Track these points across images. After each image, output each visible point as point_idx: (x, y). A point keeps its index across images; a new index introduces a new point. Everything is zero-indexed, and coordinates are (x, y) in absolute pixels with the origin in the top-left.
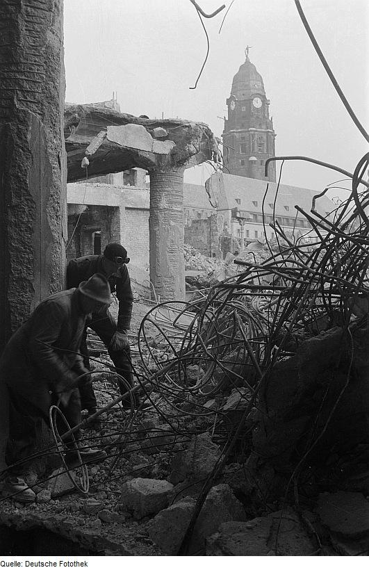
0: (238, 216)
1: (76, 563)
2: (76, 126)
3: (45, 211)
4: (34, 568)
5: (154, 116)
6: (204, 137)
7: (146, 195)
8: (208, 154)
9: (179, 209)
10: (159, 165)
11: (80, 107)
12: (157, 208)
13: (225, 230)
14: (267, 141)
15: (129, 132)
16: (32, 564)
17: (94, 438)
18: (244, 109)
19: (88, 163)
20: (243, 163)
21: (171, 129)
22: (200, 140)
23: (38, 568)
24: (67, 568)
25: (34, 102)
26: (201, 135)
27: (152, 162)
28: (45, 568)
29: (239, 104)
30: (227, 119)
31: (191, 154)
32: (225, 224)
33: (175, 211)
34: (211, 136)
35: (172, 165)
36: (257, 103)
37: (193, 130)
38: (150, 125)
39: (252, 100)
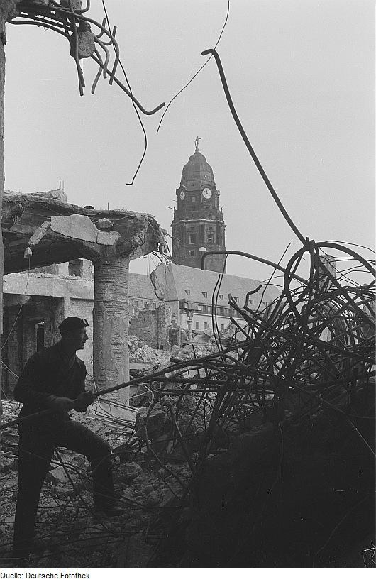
1: (77, 575)
4: (35, 580)
7: (90, 285)
8: (154, 244)
9: (125, 301)
10: (104, 256)
11: (24, 197)
13: (173, 322)
16: (32, 576)
21: (117, 220)
23: (39, 580)
24: (69, 580)
26: (146, 226)
28: (46, 580)
31: (137, 245)
32: (173, 316)
34: (157, 227)
35: (118, 256)
36: (207, 194)
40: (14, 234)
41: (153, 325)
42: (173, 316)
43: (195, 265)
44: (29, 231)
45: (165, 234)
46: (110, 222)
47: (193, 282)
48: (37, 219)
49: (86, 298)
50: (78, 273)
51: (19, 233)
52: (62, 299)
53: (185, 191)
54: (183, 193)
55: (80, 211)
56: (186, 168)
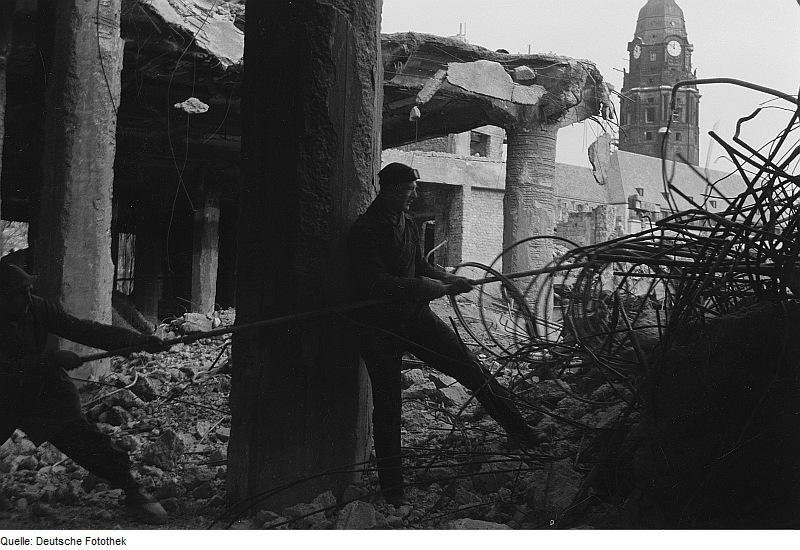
0: (638, 207)
1: (109, 540)
3: (350, 146)
4: (49, 547)
5: (515, 51)
7: (501, 171)
8: (594, 107)
10: (521, 121)
11: (411, 35)
12: (517, 182)
13: (618, 228)
14: (688, 106)
16: (46, 541)
18: (653, 57)
19: (418, 114)
20: (649, 136)
21: (541, 68)
22: (582, 85)
23: (55, 547)
24: (97, 547)
26: (584, 79)
28: (64, 547)
29: (646, 49)
30: (628, 72)
31: (569, 106)
32: (618, 220)
34: (599, 81)
35: (541, 122)
36: (674, 49)
37: (573, 71)
38: (511, 63)
39: (667, 44)
40: (398, 88)
41: (589, 233)
42: (618, 220)
43: (651, 152)
45: (610, 91)
46: (532, 71)
47: (642, 174)
48: (428, 67)
49: (494, 187)
50: (484, 152)
51: (403, 87)
52: (460, 188)
55: (490, 57)
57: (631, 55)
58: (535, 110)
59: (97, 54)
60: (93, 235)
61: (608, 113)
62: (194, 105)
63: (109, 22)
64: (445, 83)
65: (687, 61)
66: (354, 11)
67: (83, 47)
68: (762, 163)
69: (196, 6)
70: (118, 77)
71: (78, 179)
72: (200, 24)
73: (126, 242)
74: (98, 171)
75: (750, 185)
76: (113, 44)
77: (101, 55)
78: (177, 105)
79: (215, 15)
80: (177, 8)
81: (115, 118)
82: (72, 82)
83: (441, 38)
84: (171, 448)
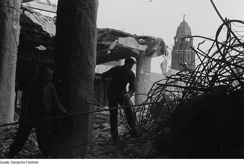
1: (33, 162)
2: (105, 37)
5: (139, 34)
6: (161, 44)
8: (163, 51)
9: (149, 75)
11: (108, 29)
14: (192, 56)
15: (128, 40)
16: (14, 162)
17: (103, 150)
19: (110, 52)
21: (146, 40)
25: (85, 9)
26: (159, 43)
27: (138, 54)
30: (174, 46)
31: (155, 51)
33: (147, 75)
34: (164, 44)
35: (146, 56)
37: (156, 41)
38: (138, 38)
40: (103, 45)
44: (109, 44)
51: (105, 45)
53: (178, 38)
54: (177, 39)
55: (131, 36)
56: (179, 28)
57: (175, 41)
58: (145, 52)
59: (12, 30)
60: (10, 84)
61: (166, 54)
62: (42, 48)
63: (16, 20)
64: (118, 44)
65: (191, 43)
66: (89, 14)
67: (8, 27)
68: (205, 55)
69: (43, 18)
70: (19, 37)
71: (6, 67)
72: (43, 23)
73: (20, 93)
74: (12, 64)
75: (202, 62)
76: (17, 27)
77: (14, 30)
78: (36, 48)
79: (49, 21)
80: (37, 19)
81: (17, 49)
82: (4, 37)
83: (116, 30)
84: (31, 145)
